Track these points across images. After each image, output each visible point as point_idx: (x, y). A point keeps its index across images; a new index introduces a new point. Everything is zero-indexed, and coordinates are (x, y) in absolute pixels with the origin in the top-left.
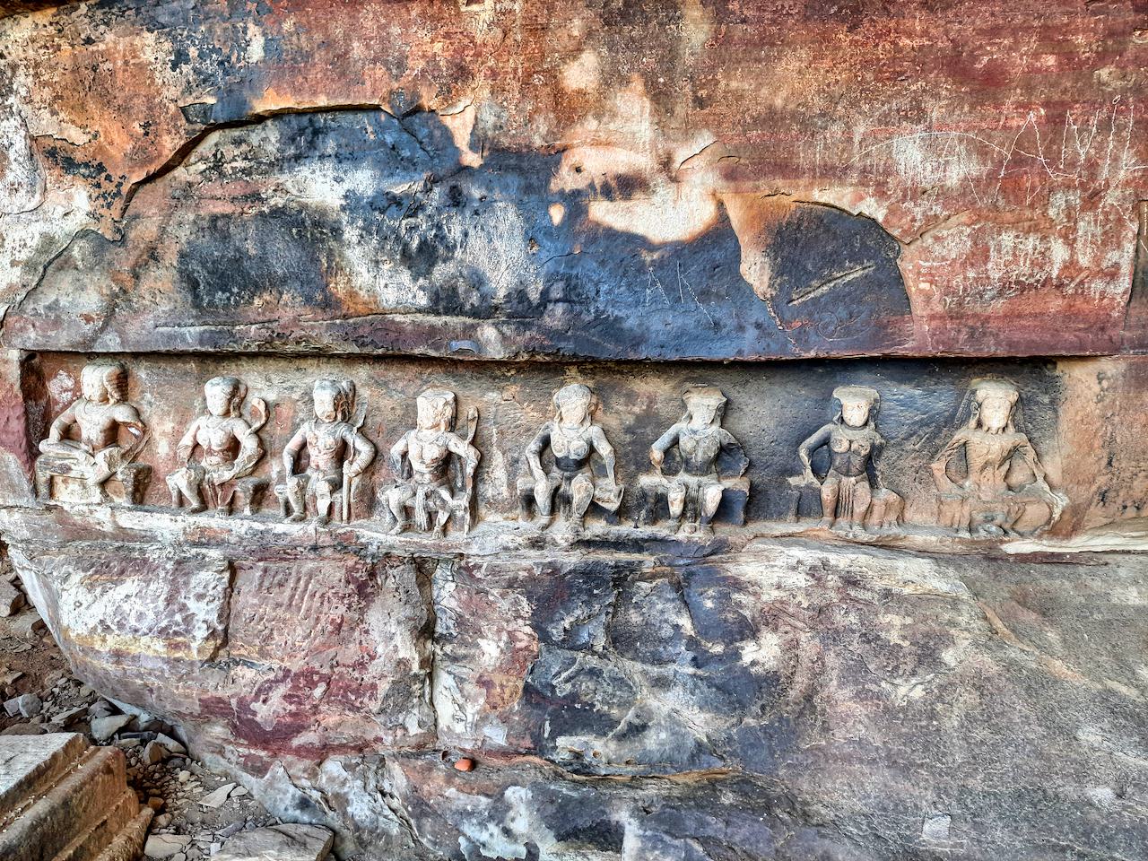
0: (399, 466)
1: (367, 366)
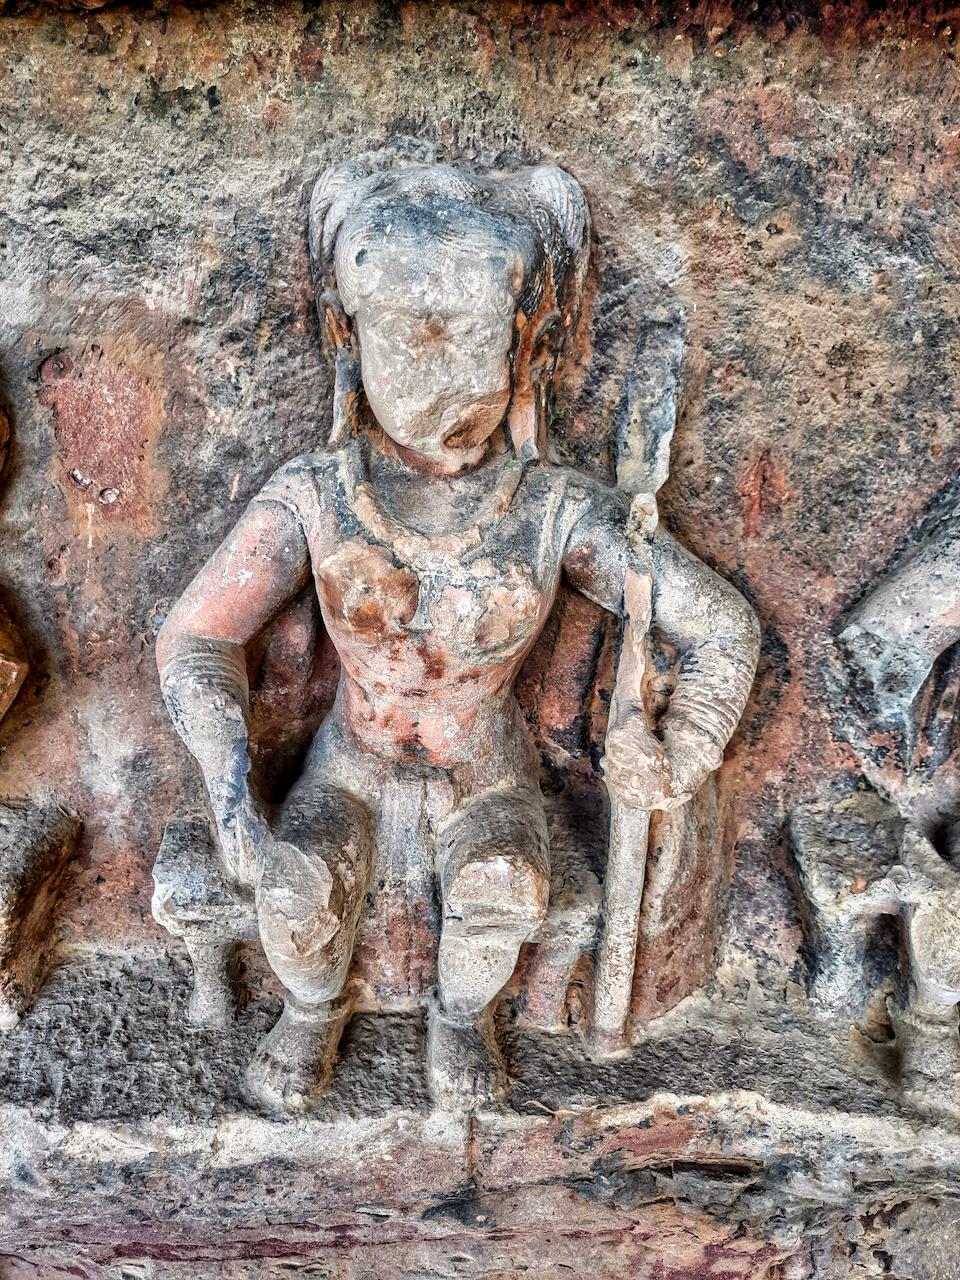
1: (680, 61)
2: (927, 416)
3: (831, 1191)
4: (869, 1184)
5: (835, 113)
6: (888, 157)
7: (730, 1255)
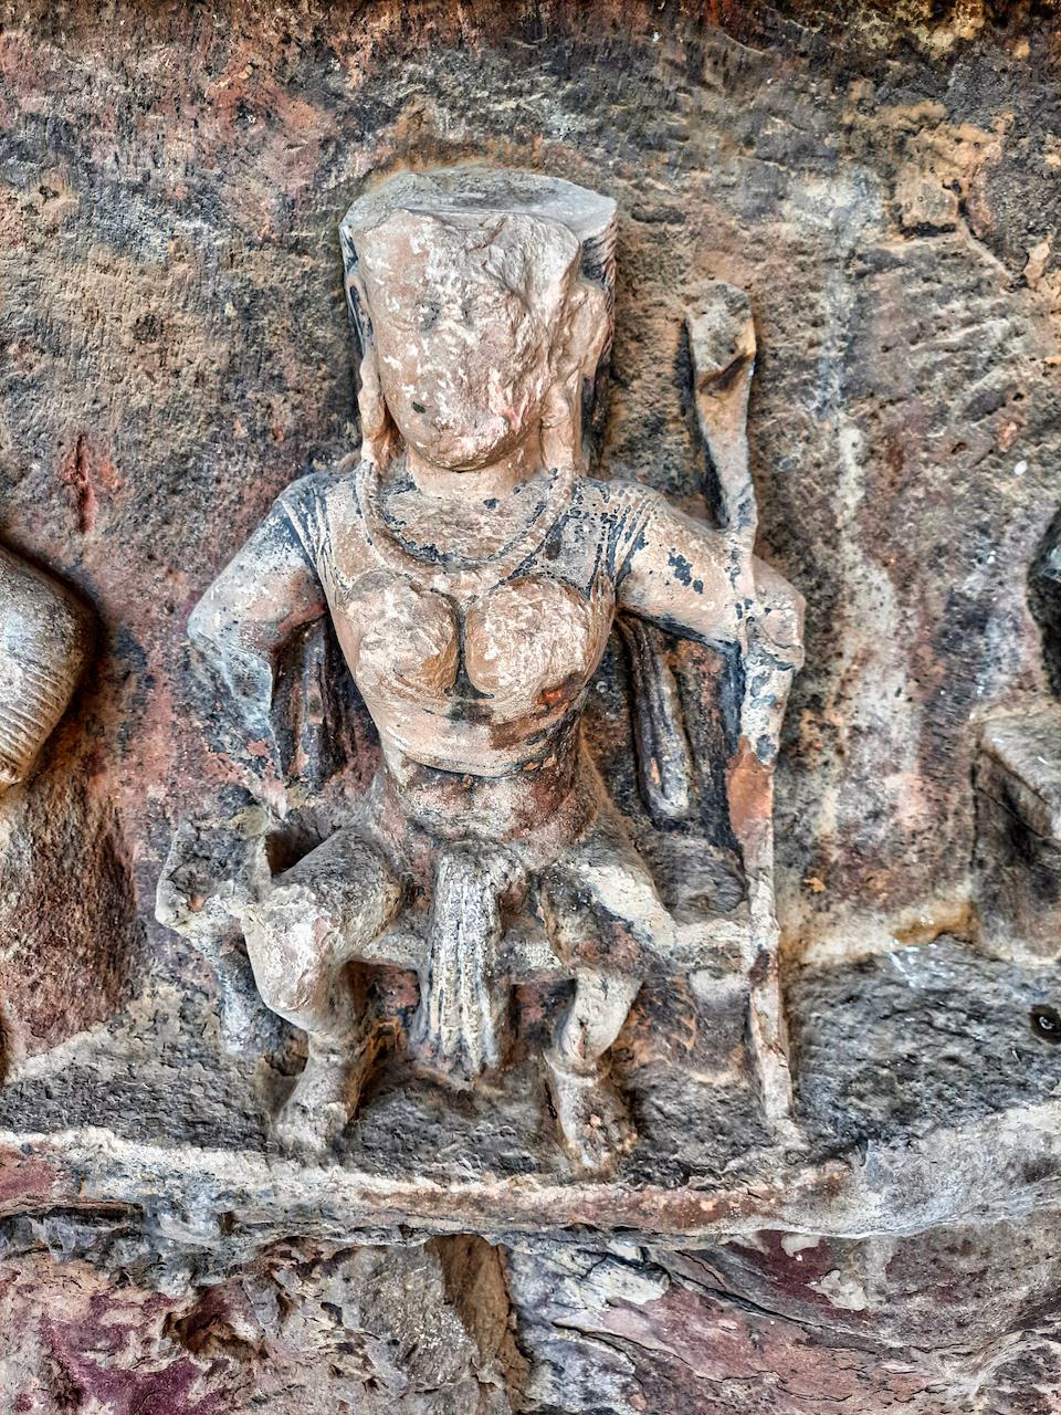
0: (258, 713)
2: (259, 396)
3: (199, 1234)
4: (249, 1227)
5: (88, 64)
6: (155, 111)
7: (117, 1306)
